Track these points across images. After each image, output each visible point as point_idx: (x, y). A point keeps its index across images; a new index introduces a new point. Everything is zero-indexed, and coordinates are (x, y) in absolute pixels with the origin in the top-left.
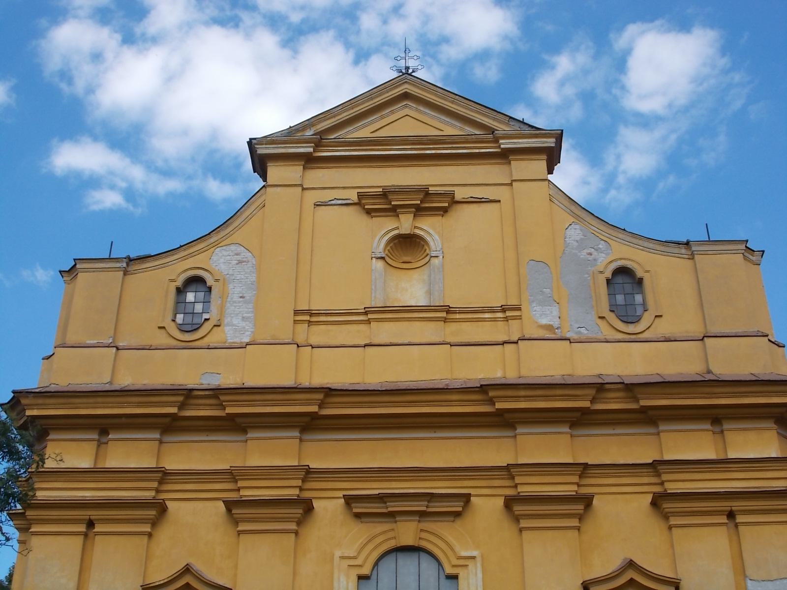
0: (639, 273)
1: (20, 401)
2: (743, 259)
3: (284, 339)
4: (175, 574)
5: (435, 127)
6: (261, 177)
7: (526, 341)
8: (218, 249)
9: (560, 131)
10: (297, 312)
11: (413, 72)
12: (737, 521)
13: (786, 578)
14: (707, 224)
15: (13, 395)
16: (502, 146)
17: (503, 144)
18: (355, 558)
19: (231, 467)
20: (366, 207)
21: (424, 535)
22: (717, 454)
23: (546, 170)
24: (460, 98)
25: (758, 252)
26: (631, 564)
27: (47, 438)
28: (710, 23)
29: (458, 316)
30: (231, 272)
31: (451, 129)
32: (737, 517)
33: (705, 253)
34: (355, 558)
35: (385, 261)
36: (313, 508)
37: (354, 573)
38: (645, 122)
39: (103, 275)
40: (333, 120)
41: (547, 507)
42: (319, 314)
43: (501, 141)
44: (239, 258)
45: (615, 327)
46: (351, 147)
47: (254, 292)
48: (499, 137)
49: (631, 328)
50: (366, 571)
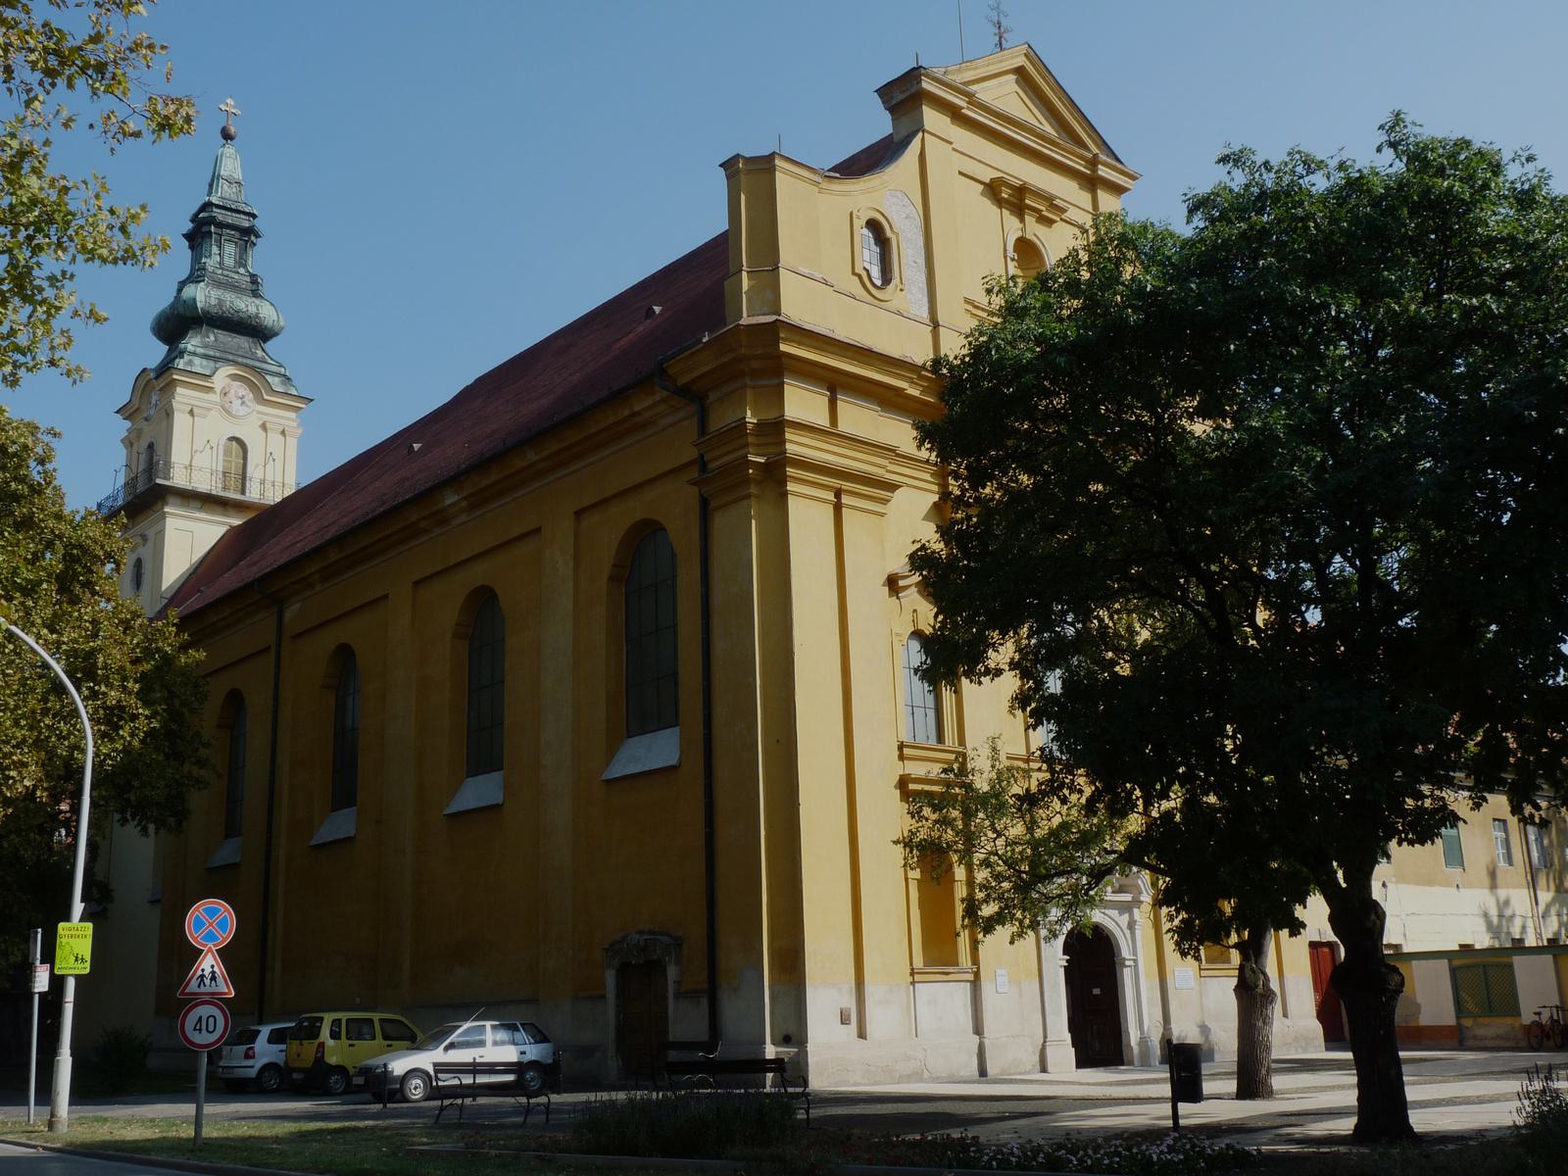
14: (960, 173)
16: (1100, 173)
17: (1102, 170)
19: (882, 515)
31: (1048, 128)
43: (1100, 166)
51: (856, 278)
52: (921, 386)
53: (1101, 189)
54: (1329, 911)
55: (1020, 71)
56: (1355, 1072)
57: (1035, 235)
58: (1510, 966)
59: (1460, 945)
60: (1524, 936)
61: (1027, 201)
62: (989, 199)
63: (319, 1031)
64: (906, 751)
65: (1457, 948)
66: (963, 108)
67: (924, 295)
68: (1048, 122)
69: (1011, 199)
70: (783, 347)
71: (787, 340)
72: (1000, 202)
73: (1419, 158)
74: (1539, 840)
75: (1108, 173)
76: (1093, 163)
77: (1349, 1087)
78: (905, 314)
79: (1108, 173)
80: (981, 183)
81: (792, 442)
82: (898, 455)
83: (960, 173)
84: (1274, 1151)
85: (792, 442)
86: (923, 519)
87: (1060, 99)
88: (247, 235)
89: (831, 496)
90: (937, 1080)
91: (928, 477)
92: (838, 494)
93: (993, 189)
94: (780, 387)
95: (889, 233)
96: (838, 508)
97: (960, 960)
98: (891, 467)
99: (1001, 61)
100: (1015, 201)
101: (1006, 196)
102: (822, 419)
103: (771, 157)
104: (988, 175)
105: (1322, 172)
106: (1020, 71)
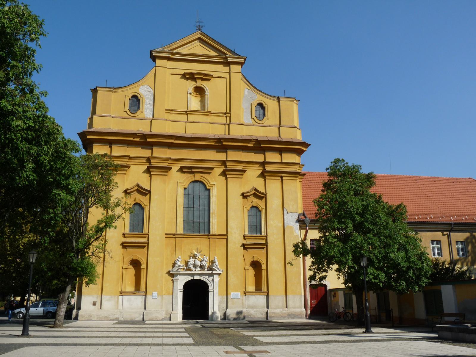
0: (264, 105)
8: (141, 87)
10: (166, 110)
11: (201, 28)
12: (152, 174)
14: (171, 74)
16: (228, 60)
17: (229, 59)
18: (183, 183)
20: (187, 77)
21: (202, 178)
26: (256, 189)
29: (213, 114)
30: (146, 95)
31: (213, 53)
32: (283, 177)
33: (283, 101)
34: (183, 183)
37: (183, 187)
39: (106, 93)
40: (177, 45)
41: (194, 163)
42: (212, 113)
43: (228, 59)
44: (148, 90)
49: (260, 122)
50: (186, 187)
51: (125, 112)
52: (214, 141)
54: (135, 273)
55: (199, 39)
57: (201, 84)
58: (439, 292)
61: (195, 76)
62: (183, 79)
68: (212, 50)
69: (191, 77)
70: (88, 137)
71: (89, 135)
72: (187, 79)
74: (195, 232)
75: (232, 60)
76: (226, 58)
77: (182, 292)
78: (168, 120)
79: (232, 60)
82: (130, 157)
83: (171, 74)
86: (219, 175)
87: (214, 43)
88: (361, 167)
89: (280, 178)
90: (301, 301)
91: (144, 161)
92: (282, 177)
93: (184, 76)
95: (139, 98)
96: (282, 181)
97: (141, 289)
98: (244, 165)
99: (189, 39)
100: (192, 77)
101: (188, 77)
102: (279, 161)
103: (96, 88)
104: (182, 72)
106: (199, 39)
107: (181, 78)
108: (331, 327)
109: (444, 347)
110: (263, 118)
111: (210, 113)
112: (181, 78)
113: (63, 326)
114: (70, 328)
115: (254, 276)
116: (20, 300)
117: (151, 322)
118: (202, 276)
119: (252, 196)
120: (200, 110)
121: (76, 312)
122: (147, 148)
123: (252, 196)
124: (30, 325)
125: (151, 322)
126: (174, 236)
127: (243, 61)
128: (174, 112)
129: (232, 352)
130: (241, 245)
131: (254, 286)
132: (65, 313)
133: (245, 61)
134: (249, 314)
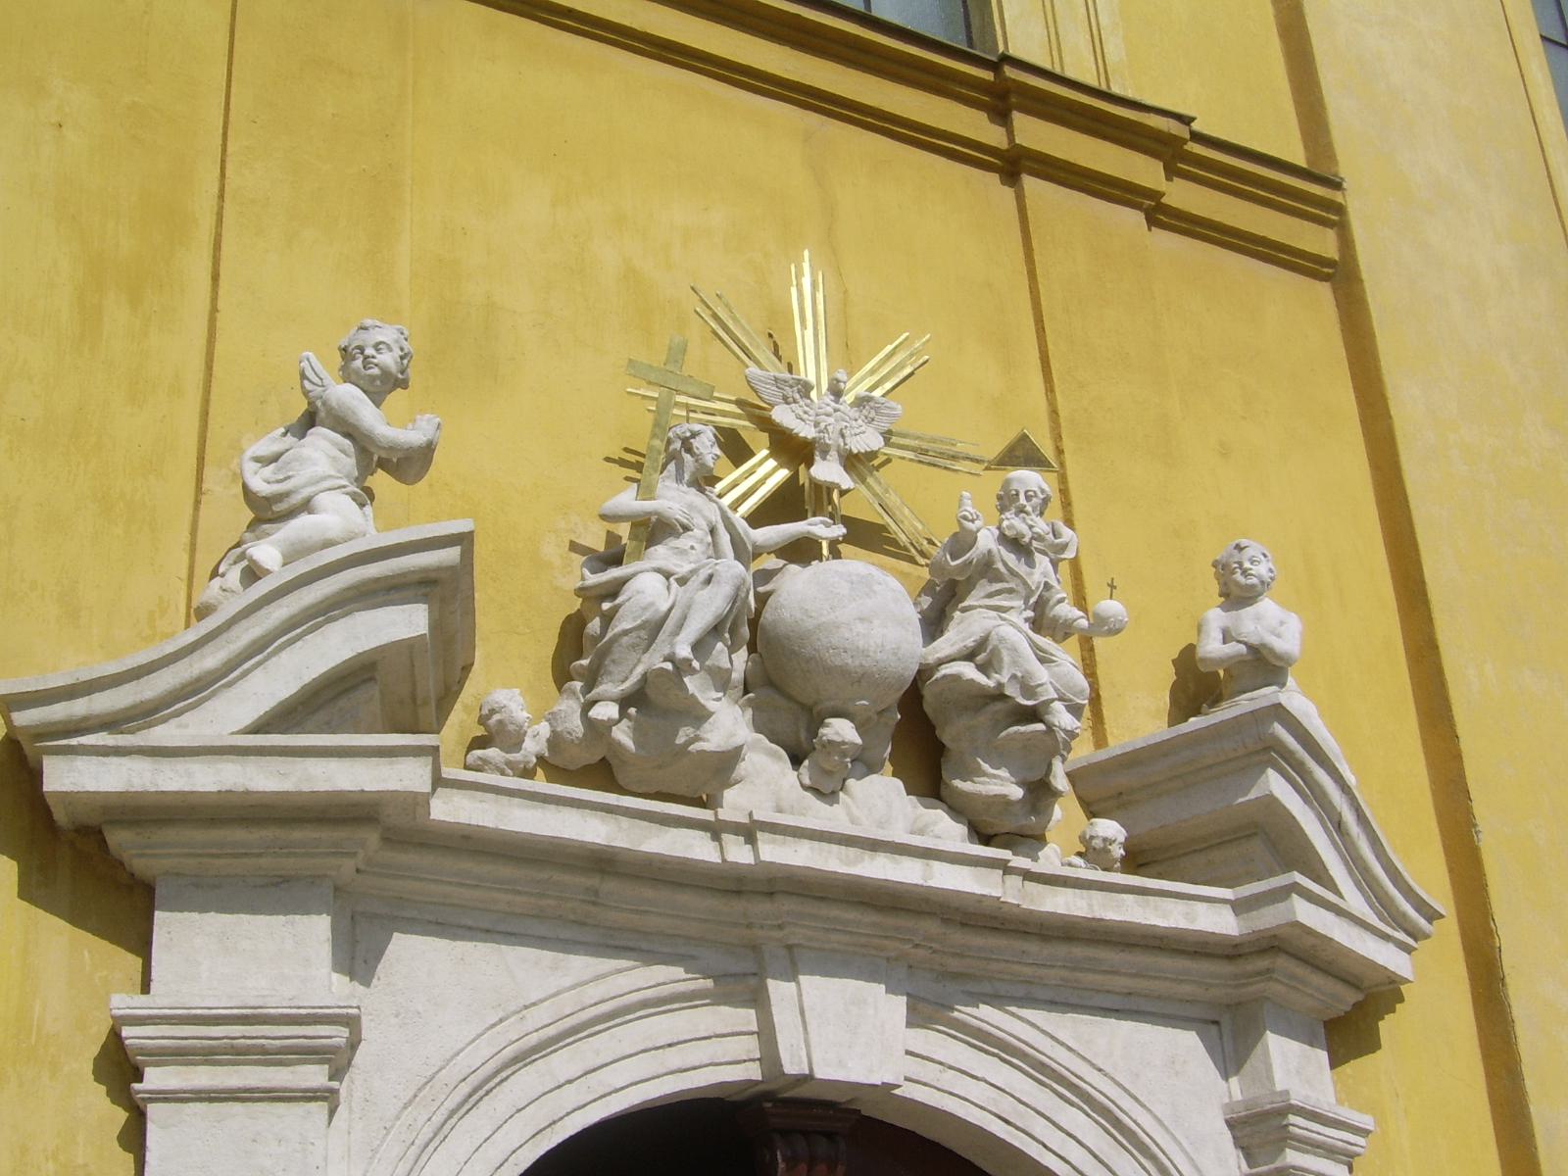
1: (1034, 611)
2: (1233, 1146)
3: (1339, 1115)
4: (1101, 1092)
5: (1552, 186)
6: (219, 791)
7: (1527, 83)
9: (1352, 997)
13: (1043, 2)
15: (577, 603)
19: (626, 450)
22: (1308, 160)
23: (153, 969)
24: (563, 1063)
25: (470, 1047)
27: (1007, 1008)
28: (1267, 767)
35: (1287, 953)
36: (944, 746)
38: (716, 814)
45: (1534, 128)
46: (976, 151)
47: (1221, 673)
48: (1024, 90)
53: (1276, 1031)
54: (1194, 1033)
56: (127, 1042)
59: (978, 1007)
60: (796, 773)
63: (1081, 648)
64: (894, 439)
65: (981, 1006)
66: (1185, 142)
67: (1112, 733)
73: (340, 407)
77: (1230, 1097)
80: (753, 1060)
81: (774, 470)
83: (909, 1053)
84: (1295, 778)
85: (774, 470)
90: (1082, 1020)
94: (763, 1077)
105: (465, 717)
107: (722, 807)
108: (1074, 1000)
109: (753, 369)
110: (996, 835)
111: (637, 910)
112: (722, 807)
113: (965, 1013)
114: (768, 481)
115: (883, 1083)
116: (104, 1084)
117: (465, 707)
118: (987, 1015)
119: (733, 656)
120: (430, 759)
121: (929, 580)
122: (576, 943)
123: (733, 656)
124: (425, 634)
125: (466, 708)
126: (991, 134)
127: (340, 1041)
128: (1052, 30)
129: (1093, 695)
130: (1170, 183)
131: (572, 956)
132: (139, 666)
133: (468, 556)
134: (894, 646)
